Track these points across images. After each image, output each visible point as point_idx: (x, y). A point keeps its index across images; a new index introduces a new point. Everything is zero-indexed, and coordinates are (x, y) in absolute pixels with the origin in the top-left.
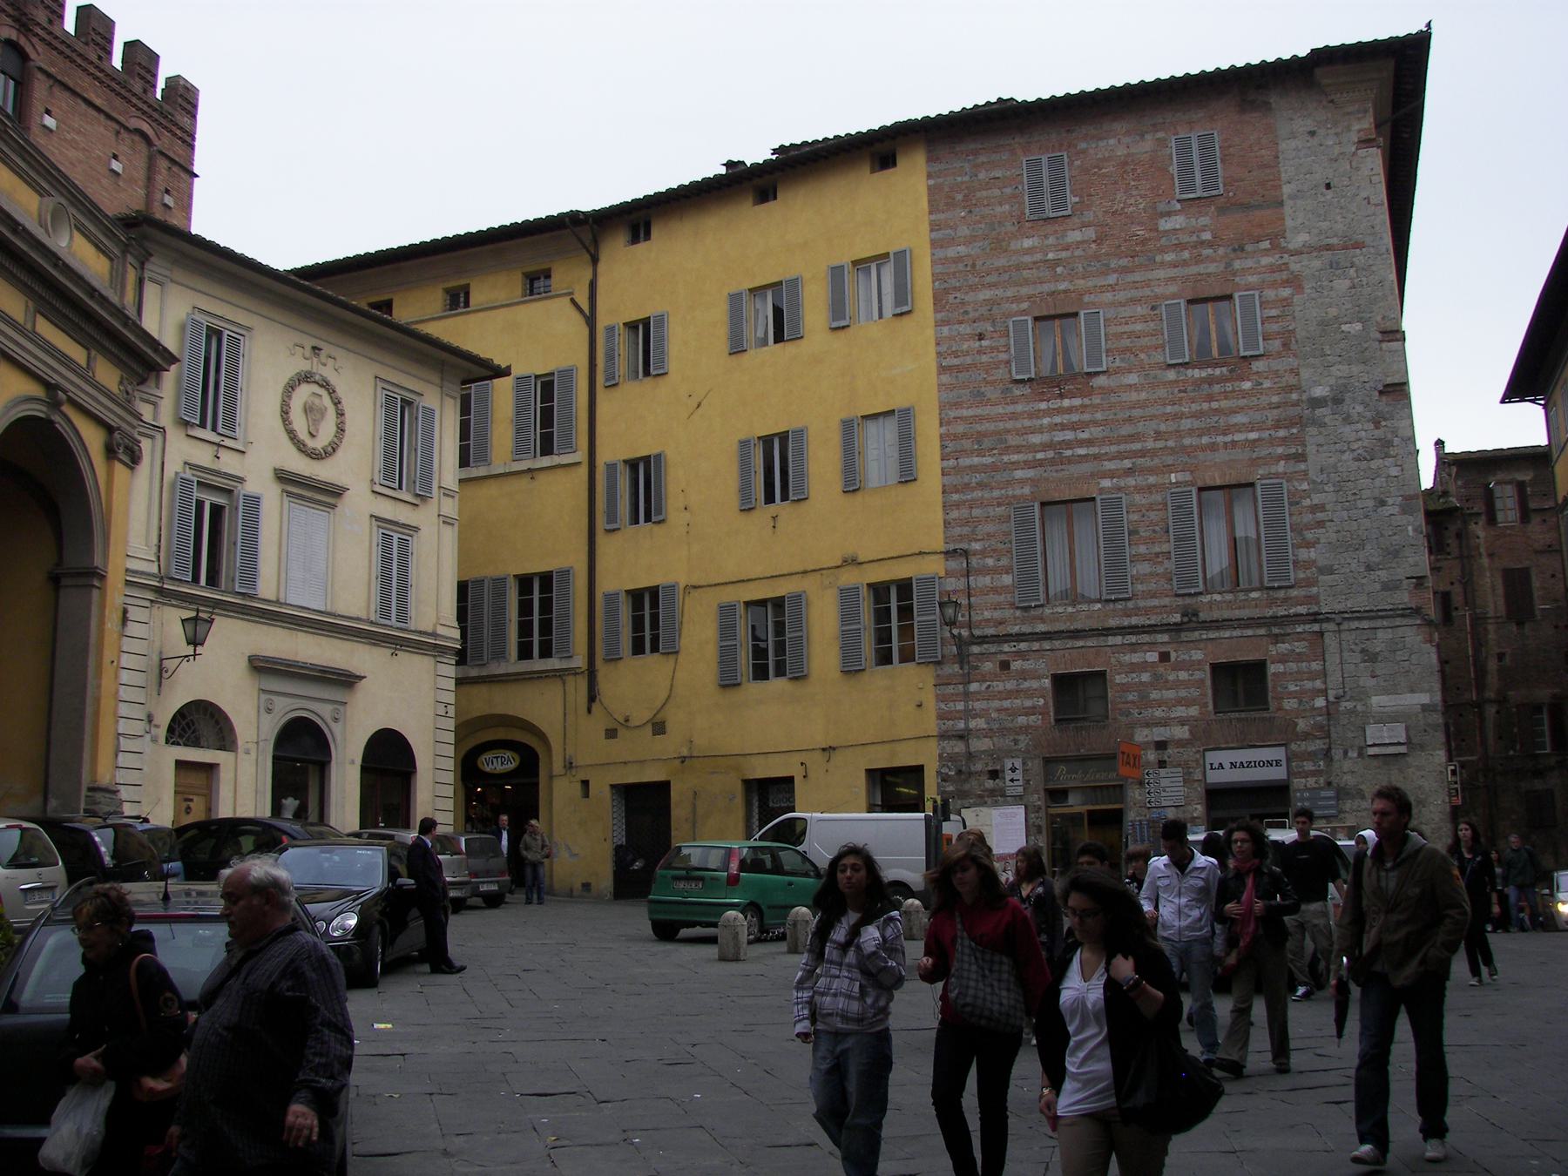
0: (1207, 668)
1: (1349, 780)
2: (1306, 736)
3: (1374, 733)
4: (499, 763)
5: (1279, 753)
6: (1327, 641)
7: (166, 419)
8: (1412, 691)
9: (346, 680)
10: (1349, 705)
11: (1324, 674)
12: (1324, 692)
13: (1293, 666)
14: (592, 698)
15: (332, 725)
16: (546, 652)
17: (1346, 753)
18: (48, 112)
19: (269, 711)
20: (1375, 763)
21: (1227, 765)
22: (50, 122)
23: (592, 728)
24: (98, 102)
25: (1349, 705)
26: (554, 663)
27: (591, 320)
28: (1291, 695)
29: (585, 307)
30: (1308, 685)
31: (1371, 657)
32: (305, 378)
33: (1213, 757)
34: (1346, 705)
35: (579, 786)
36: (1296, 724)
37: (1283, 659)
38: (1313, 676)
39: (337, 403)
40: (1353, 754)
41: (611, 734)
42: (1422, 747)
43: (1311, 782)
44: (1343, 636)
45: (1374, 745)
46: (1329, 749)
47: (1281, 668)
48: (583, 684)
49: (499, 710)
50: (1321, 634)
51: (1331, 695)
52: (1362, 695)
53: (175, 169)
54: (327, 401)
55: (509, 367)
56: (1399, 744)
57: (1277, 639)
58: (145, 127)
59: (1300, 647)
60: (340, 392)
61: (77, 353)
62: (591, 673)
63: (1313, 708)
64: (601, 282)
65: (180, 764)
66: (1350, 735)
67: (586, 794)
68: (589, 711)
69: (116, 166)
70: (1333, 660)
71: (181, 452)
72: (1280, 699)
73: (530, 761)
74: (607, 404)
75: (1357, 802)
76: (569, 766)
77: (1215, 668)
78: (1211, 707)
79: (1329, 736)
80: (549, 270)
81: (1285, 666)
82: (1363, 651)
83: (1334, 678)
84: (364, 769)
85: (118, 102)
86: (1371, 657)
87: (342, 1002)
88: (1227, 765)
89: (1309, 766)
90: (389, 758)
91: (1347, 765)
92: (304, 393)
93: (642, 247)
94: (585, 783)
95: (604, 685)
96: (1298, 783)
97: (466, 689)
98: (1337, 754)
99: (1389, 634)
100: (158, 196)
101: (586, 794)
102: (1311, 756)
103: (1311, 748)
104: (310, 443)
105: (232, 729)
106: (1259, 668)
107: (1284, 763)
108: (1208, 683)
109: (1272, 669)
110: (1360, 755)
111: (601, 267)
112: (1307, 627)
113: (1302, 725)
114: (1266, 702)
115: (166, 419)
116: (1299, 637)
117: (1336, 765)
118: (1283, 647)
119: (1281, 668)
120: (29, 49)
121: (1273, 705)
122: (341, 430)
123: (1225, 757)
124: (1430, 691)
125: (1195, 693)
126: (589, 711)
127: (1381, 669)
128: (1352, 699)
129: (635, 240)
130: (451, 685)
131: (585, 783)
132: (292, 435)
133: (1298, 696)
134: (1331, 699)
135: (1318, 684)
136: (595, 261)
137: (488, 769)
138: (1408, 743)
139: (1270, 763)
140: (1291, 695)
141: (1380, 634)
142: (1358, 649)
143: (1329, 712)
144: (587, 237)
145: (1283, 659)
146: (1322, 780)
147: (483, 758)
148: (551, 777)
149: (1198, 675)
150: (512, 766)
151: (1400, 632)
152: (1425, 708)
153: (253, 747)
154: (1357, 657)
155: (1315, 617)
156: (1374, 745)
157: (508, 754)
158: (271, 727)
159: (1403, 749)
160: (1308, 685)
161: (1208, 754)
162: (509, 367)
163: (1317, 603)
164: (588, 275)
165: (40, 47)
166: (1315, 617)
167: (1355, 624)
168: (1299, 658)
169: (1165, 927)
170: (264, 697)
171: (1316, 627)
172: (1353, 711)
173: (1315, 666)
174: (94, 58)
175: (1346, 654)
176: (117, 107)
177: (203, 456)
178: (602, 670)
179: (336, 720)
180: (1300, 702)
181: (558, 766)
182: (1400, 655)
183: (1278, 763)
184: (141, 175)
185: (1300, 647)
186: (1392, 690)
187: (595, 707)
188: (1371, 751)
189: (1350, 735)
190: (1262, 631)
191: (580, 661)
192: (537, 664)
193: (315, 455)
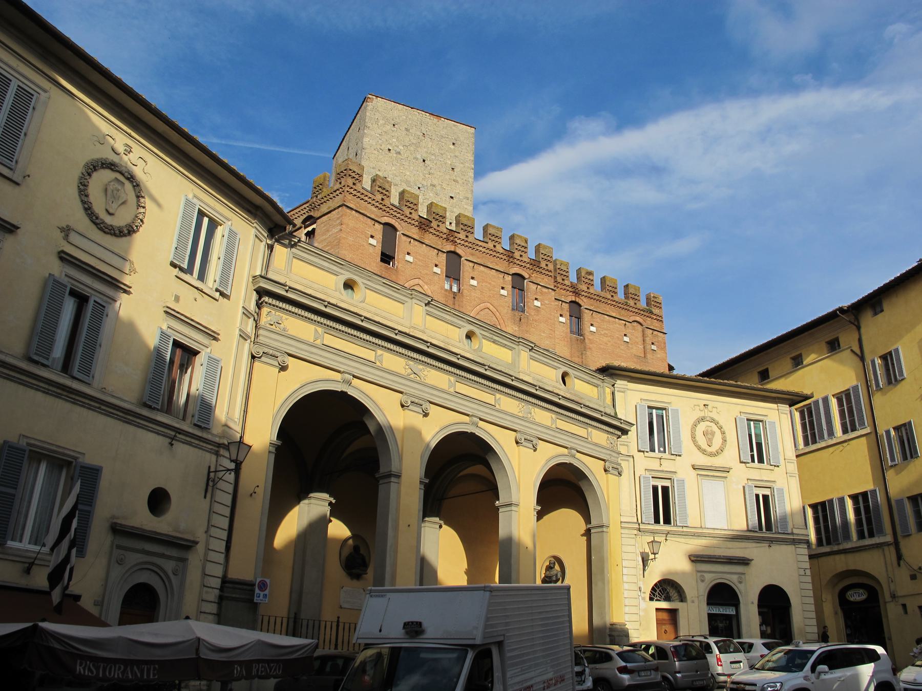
4: (857, 596)
7: (634, 451)
9: (744, 562)
14: (899, 557)
15: (739, 585)
16: (871, 535)
18: (592, 325)
19: (703, 581)
22: (593, 329)
23: (903, 575)
24: (614, 315)
26: (876, 540)
27: (862, 358)
29: (858, 352)
32: (703, 419)
35: (901, 607)
39: (720, 428)
41: (913, 577)
48: (892, 549)
49: (852, 567)
53: (655, 333)
54: (715, 428)
55: (812, 393)
58: (638, 319)
60: (721, 423)
61: (582, 432)
62: (896, 544)
64: (864, 338)
65: (657, 609)
67: (906, 612)
68: (899, 565)
69: (626, 339)
71: (645, 463)
73: (873, 592)
74: (877, 400)
76: (893, 596)
80: (837, 340)
84: (759, 606)
85: (623, 312)
90: (774, 602)
92: (702, 427)
93: (880, 316)
94: (904, 606)
95: (904, 551)
97: (815, 561)
100: (648, 347)
101: (906, 612)
104: (709, 449)
105: (684, 591)
111: (863, 330)
115: (634, 451)
120: (580, 302)
122: (725, 441)
126: (899, 565)
129: (876, 314)
130: (807, 559)
131: (904, 606)
132: (699, 448)
136: (859, 328)
137: (852, 599)
144: (852, 318)
147: (849, 593)
148: (885, 603)
150: (864, 597)
153: (696, 600)
157: (861, 591)
158: (704, 590)
162: (812, 393)
164: (857, 337)
165: (585, 300)
170: (699, 574)
174: (609, 297)
176: (624, 314)
177: (655, 465)
178: (903, 543)
179: (740, 582)
181: (887, 597)
184: (640, 339)
187: (902, 562)
191: (889, 538)
192: (868, 542)
193: (711, 455)
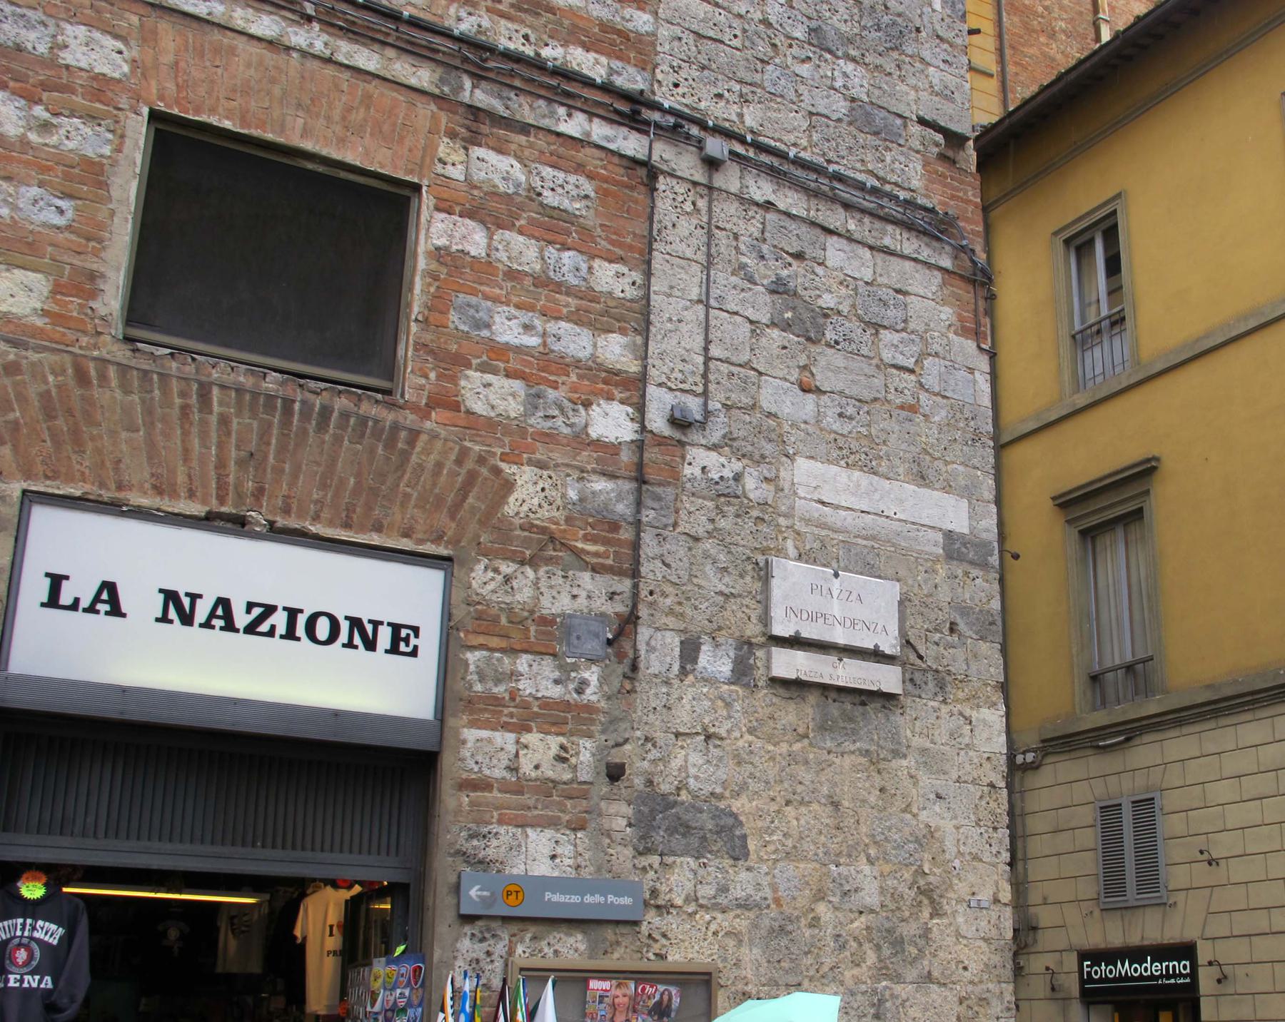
0: (138, 130)
1: (692, 769)
2: (543, 546)
3: (802, 595)
5: (410, 594)
6: (663, 205)
8: (922, 479)
10: (718, 465)
11: (638, 318)
12: (633, 388)
13: (522, 250)
17: (690, 651)
20: (793, 714)
21: (141, 601)
25: (718, 465)
28: (498, 358)
30: (575, 342)
31: (807, 324)
33: (69, 543)
34: (702, 461)
36: (508, 486)
37: (489, 209)
38: (597, 313)
40: (716, 662)
42: (942, 681)
43: (540, 751)
44: (727, 211)
45: (796, 642)
46: (628, 623)
47: (474, 239)
50: (647, 172)
51: (659, 404)
52: (766, 443)
56: (876, 655)
57: (477, 126)
59: (566, 191)
63: (581, 440)
66: (713, 582)
70: (676, 286)
72: (453, 364)
75: (716, 867)
77: (175, 142)
78: (112, 300)
79: (635, 574)
81: (480, 219)
82: (778, 288)
83: (677, 342)
86: (807, 324)
87: (819, 981)
88: (141, 601)
89: (537, 679)
91: (690, 705)
96: (479, 749)
98: (658, 647)
99: (863, 265)
102: (547, 636)
103: (558, 602)
106: (384, 208)
107: (429, 643)
108: (127, 189)
109: (435, 231)
110: (742, 672)
112: (600, 131)
113: (528, 494)
114: (389, 369)
116: (567, 152)
117: (650, 694)
118: (496, 167)
119: (474, 239)
121: (416, 381)
123: (150, 556)
124: (968, 492)
125: (43, 210)
127: (831, 368)
128: (727, 443)
133: (539, 369)
134: (657, 422)
135: (615, 350)
138: (907, 656)
139: (362, 633)
140: (498, 358)
141: (835, 252)
142: (767, 272)
143: (647, 466)
145: (489, 209)
146: (586, 753)
149: (79, 138)
151: (897, 271)
152: (955, 547)
154: (761, 307)
155: (632, 110)
156: (796, 642)
159: (887, 679)
160: (575, 342)
161: (42, 517)
163: (647, 64)
166: (632, 110)
167: (762, 189)
168: (554, 227)
169: (1022, 779)
171: (631, 144)
172: (725, 494)
173: (611, 279)
175: (723, 277)
180: (534, 401)
182: (891, 346)
183: (403, 639)
185: (566, 191)
186: (861, 455)
188: (788, 664)
189: (713, 582)
190: (423, 76)
